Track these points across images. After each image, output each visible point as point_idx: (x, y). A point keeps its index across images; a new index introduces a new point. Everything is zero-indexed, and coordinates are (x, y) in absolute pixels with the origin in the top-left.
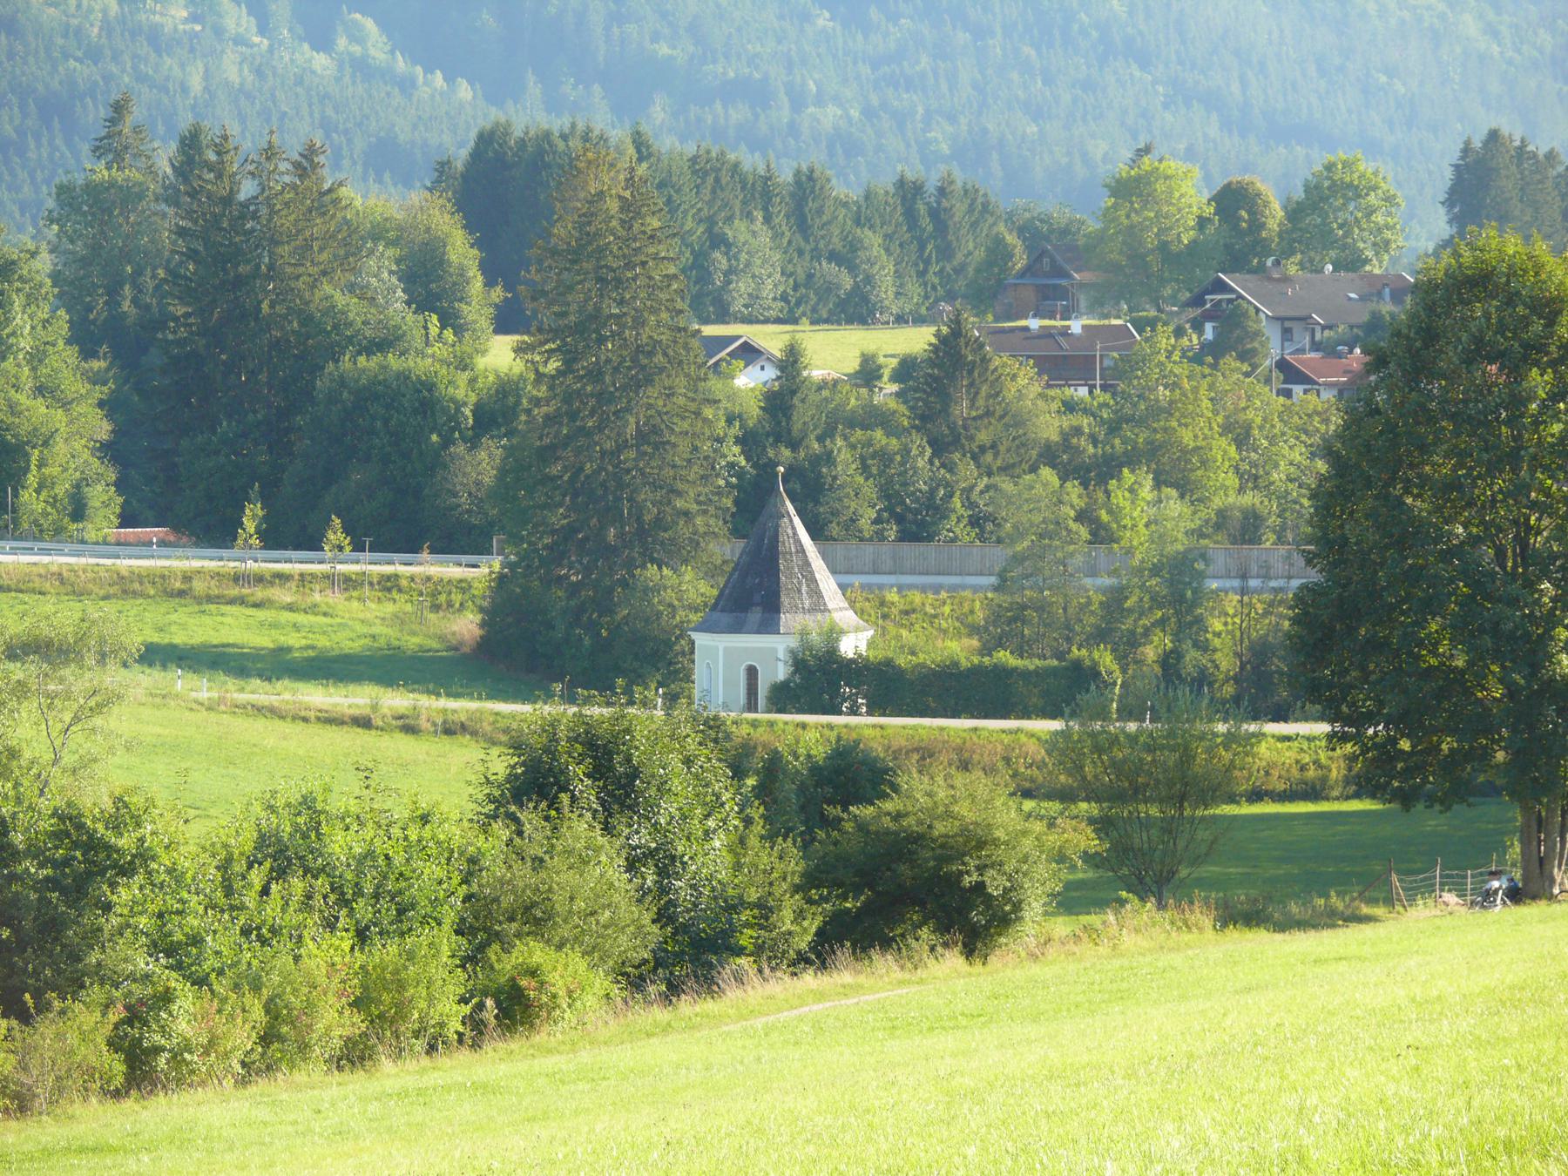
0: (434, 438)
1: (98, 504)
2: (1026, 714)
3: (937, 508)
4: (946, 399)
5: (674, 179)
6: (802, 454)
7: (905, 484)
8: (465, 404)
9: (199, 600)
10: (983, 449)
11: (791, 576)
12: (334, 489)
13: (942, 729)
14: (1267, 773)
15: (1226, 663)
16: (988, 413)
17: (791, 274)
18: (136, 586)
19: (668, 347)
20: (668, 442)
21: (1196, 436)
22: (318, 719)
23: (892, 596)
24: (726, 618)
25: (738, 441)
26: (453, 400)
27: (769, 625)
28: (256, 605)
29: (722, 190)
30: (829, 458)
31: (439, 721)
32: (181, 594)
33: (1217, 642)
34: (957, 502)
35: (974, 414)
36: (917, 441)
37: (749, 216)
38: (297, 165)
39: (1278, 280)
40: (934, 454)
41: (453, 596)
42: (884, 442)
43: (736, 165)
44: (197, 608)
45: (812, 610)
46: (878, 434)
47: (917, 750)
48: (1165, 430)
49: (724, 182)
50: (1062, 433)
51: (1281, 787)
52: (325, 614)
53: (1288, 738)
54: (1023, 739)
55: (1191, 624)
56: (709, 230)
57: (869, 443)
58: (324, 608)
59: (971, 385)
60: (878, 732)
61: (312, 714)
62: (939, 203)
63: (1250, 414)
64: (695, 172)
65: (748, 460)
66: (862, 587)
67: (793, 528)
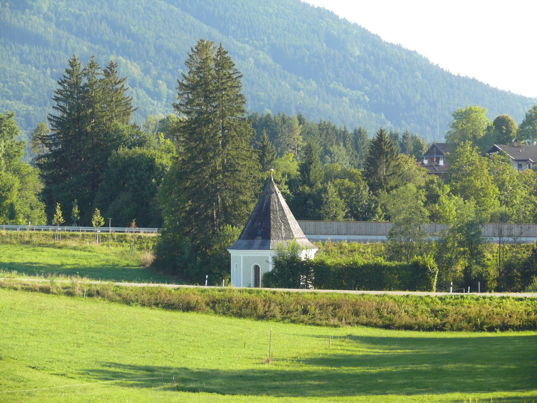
0: (154, 181)
1: (36, 217)
2: (390, 288)
3: (372, 212)
4: (376, 166)
5: (313, 131)
6: (314, 190)
7: (358, 202)
8: (166, 167)
9: (34, 245)
10: (392, 188)
11: (276, 221)
12: (113, 203)
13: (345, 295)
14: (510, 317)
15: (493, 272)
16: (394, 173)
17: (353, 164)
18: (8, 240)
19: (236, 126)
20: (237, 170)
21: (482, 184)
22: (22, 288)
23: (345, 244)
24: (245, 242)
25: (286, 183)
26: (161, 164)
27: (265, 246)
28: (60, 248)
29: (329, 135)
30: (325, 190)
31: (86, 289)
32: (28, 243)
33: (489, 263)
34: (379, 210)
35: (388, 173)
36: (363, 184)
37: (339, 144)
38: (105, 71)
39: (516, 147)
40: (370, 190)
41: (149, 244)
42: (349, 184)
43: (334, 127)
44: (32, 248)
45: (286, 238)
46: (347, 181)
47: (332, 305)
48: (469, 181)
49: (330, 133)
50: (426, 183)
51: (518, 323)
52: (89, 251)
53: (521, 299)
54: (387, 299)
55: (477, 254)
56: (325, 148)
58: (89, 249)
59: (387, 161)
60: (312, 296)
61: (19, 286)
62: (403, 141)
63: (505, 176)
64: (319, 129)
65: (291, 191)
67: (278, 198)
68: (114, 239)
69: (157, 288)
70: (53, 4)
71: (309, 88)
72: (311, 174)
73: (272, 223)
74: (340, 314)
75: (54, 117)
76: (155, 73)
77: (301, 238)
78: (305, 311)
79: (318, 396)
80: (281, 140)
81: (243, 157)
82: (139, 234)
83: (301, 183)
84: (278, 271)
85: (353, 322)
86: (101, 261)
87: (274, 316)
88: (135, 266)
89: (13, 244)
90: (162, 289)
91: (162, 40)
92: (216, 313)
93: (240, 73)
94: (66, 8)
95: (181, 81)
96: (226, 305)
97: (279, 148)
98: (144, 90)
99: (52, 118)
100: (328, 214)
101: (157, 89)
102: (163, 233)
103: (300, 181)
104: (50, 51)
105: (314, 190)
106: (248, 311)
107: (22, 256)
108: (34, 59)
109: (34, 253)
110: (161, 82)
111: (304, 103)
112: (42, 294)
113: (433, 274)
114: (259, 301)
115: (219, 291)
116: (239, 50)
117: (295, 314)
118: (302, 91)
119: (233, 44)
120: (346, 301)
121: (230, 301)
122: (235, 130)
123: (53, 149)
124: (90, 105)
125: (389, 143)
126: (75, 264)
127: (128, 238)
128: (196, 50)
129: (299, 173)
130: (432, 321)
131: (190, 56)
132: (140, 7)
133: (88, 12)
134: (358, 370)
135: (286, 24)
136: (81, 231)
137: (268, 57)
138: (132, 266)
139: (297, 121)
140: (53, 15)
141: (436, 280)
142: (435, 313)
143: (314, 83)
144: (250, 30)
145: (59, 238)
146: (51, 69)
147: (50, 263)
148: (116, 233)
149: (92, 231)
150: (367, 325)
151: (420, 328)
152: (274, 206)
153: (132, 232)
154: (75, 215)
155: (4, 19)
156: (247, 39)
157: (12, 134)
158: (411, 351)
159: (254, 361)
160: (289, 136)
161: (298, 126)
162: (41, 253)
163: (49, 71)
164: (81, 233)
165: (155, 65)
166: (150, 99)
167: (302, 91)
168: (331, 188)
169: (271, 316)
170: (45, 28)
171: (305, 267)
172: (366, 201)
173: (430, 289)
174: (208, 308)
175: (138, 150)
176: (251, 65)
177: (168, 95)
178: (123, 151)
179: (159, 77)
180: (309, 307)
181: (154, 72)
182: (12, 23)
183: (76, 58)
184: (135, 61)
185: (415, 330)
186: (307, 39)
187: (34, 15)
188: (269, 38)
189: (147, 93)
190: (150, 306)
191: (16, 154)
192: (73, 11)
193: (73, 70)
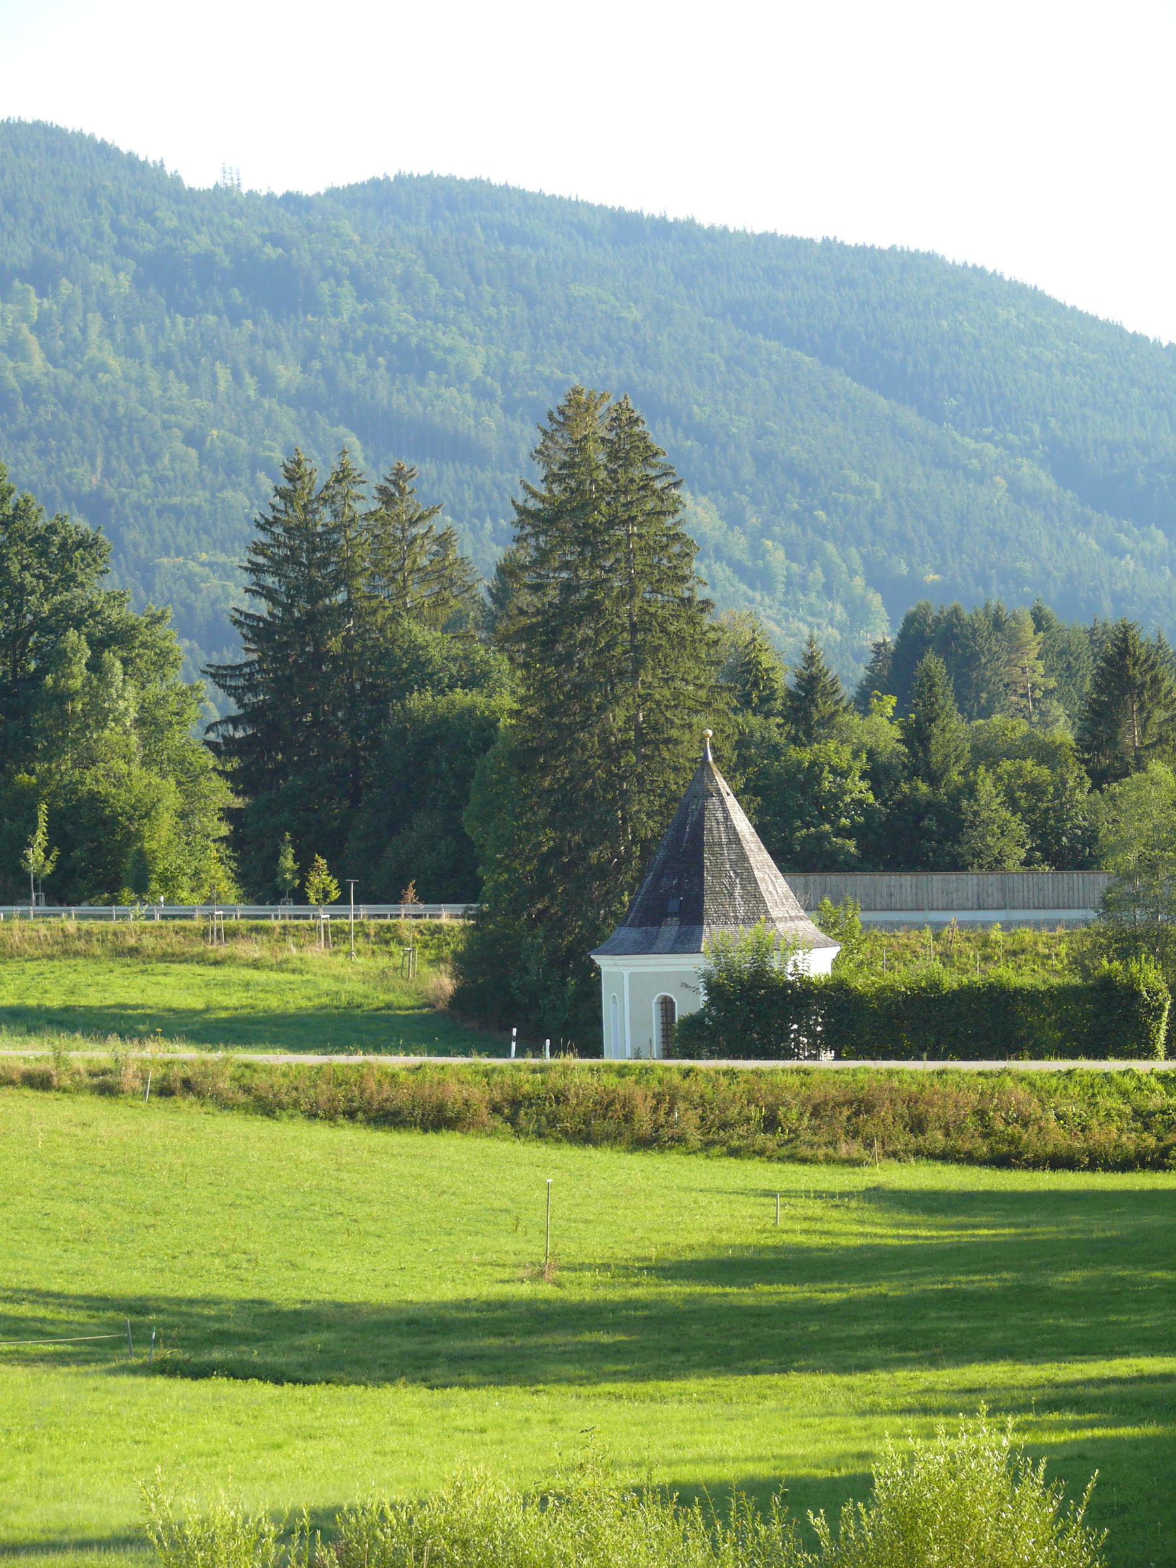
5: (1073, 648)
11: (720, 873)
13: (891, 1073)
18: (80, 945)
23: (996, 934)
27: (686, 943)
28: (216, 963)
30: (970, 790)
35: (1147, 742)
38: (382, 490)
46: (1029, 764)
52: (294, 971)
54: (1009, 1083)
57: (1019, 773)
58: (297, 964)
59: (1141, 709)
60: (795, 1080)
64: (1092, 642)
66: (962, 925)
67: (725, 811)
68: (367, 936)
69: (357, 1069)
70: (497, 355)
71: (1148, 546)
72: (933, 748)
73: (708, 877)
74: (869, 1129)
75: (248, 616)
76: (754, 521)
77: (791, 919)
78: (771, 1123)
79: (570, 1381)
80: (988, 673)
81: (689, 703)
82: (436, 921)
83: (905, 773)
84: (719, 1011)
85: (906, 1152)
86: (319, 996)
87: (679, 1140)
88: (408, 1009)
89: (94, 956)
90: (369, 1065)
91: (771, 438)
92: (518, 1132)
93: (674, 475)
94: (528, 367)
95: (520, 502)
96: (548, 1109)
97: (984, 695)
98: (728, 565)
99: (242, 619)
100: (977, 854)
101: (760, 562)
102: (480, 917)
103: (905, 766)
104: (489, 475)
105: (942, 791)
106: (609, 1126)
107: (105, 988)
108: (450, 495)
109: (142, 981)
110: (769, 543)
111: (1134, 585)
112: (28, 1092)
113: (1155, 1009)
114: (638, 1101)
115: (534, 1071)
116: (969, 458)
117: (741, 1130)
118: (1129, 556)
119: (954, 443)
120: (891, 1089)
121: (560, 1097)
122: (664, 631)
123: (246, 701)
124: (342, 578)
125: (1146, 661)
126: (242, 1007)
127: (406, 934)
128: (561, 419)
129: (902, 748)
130: (1130, 1143)
131: (545, 433)
132: (717, 357)
133: (586, 373)
134: (792, 1293)
135: (1086, 388)
136: (279, 916)
137: (1042, 474)
138: (399, 1008)
139: (1030, 625)
140: (497, 386)
141: (1164, 1026)
142: (1144, 1118)
143: (1160, 535)
144: (998, 408)
145: (219, 937)
146: (494, 519)
147: (175, 1005)
148: (373, 922)
149: (306, 917)
150: (945, 1157)
151: (1096, 1162)
152: (714, 832)
153: (408, 918)
154: (288, 876)
155: (373, 397)
156: (988, 430)
157: (161, 667)
158: (1013, 1231)
159: (506, 1274)
160: (1008, 663)
161: (1031, 634)
162: (161, 978)
163: (488, 525)
164: (281, 922)
165: (756, 501)
166: (744, 587)
167: (1129, 556)
168: (986, 786)
169: (672, 1139)
170: (477, 416)
171: (801, 998)
172: (1084, 819)
173: (1146, 1051)
174: (498, 1122)
175: (461, 697)
176: (999, 494)
177: (788, 577)
178: (419, 701)
179: (765, 531)
180: (782, 1109)
181: (754, 520)
182: (394, 406)
183: (302, 457)
184: (704, 493)
185: (1083, 1169)
186: (1143, 424)
187: (448, 384)
188: (1045, 426)
189: (734, 572)
190: (330, 1117)
191: (175, 719)
192: (547, 372)
193: (295, 491)
